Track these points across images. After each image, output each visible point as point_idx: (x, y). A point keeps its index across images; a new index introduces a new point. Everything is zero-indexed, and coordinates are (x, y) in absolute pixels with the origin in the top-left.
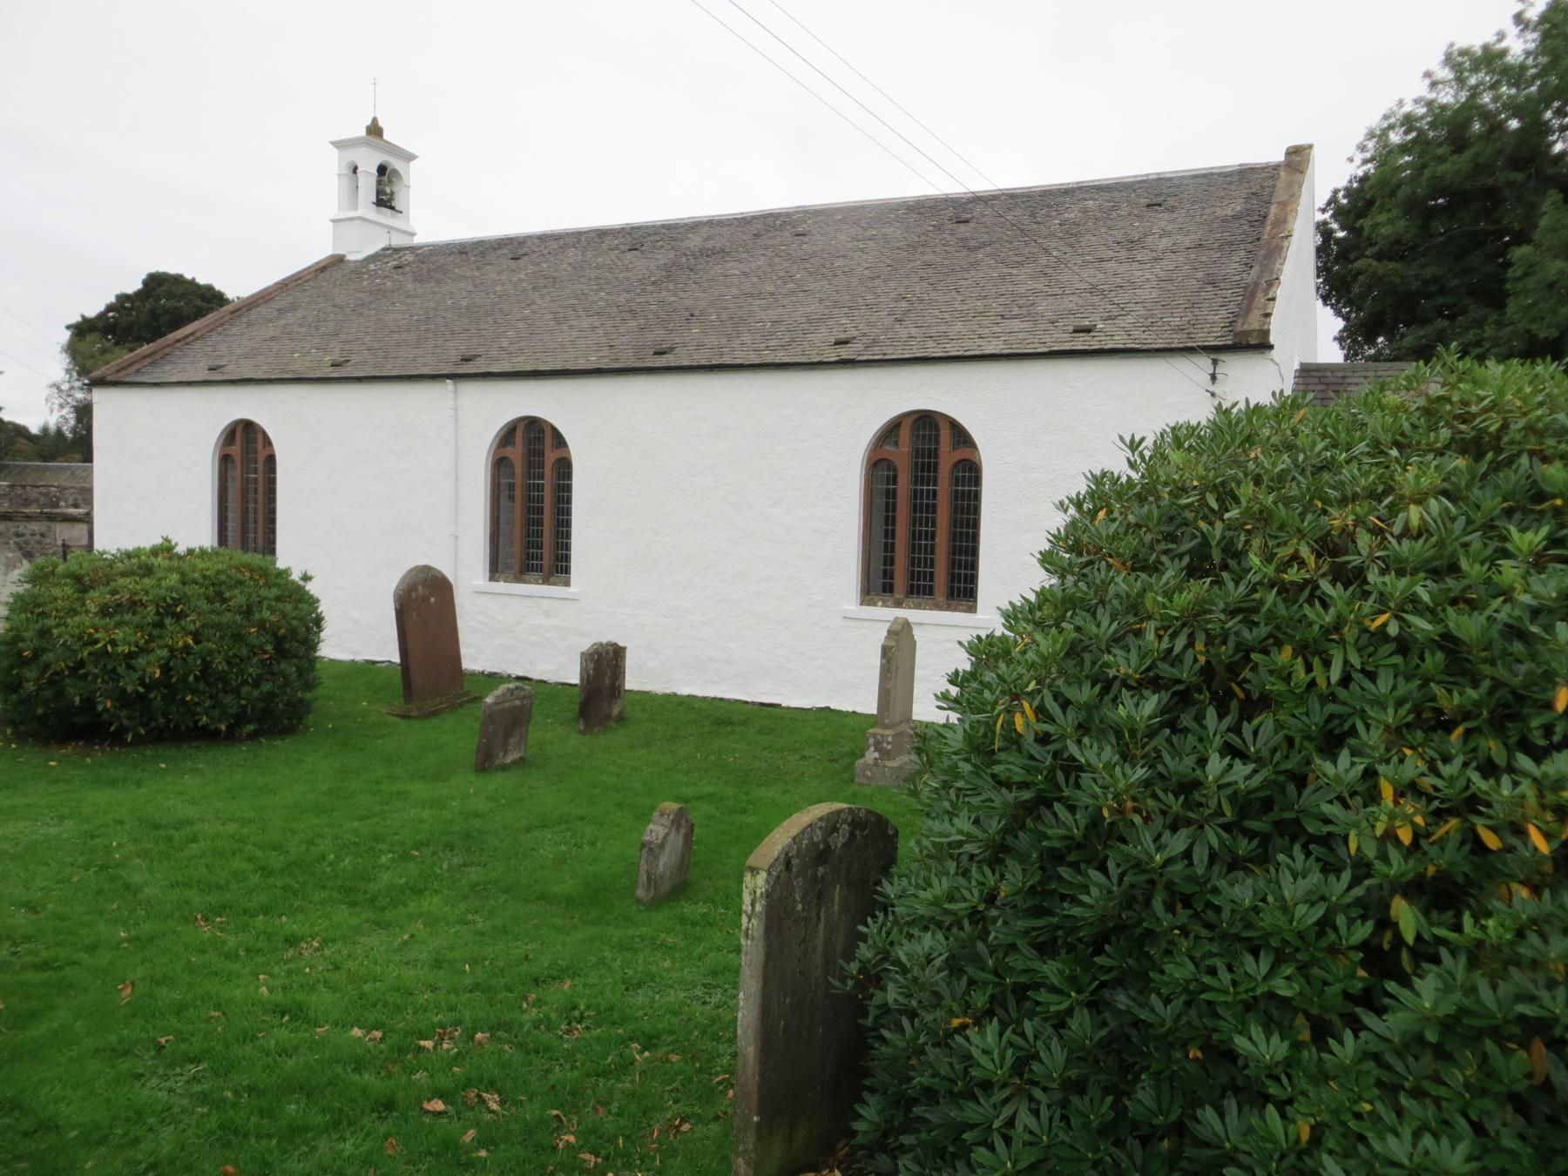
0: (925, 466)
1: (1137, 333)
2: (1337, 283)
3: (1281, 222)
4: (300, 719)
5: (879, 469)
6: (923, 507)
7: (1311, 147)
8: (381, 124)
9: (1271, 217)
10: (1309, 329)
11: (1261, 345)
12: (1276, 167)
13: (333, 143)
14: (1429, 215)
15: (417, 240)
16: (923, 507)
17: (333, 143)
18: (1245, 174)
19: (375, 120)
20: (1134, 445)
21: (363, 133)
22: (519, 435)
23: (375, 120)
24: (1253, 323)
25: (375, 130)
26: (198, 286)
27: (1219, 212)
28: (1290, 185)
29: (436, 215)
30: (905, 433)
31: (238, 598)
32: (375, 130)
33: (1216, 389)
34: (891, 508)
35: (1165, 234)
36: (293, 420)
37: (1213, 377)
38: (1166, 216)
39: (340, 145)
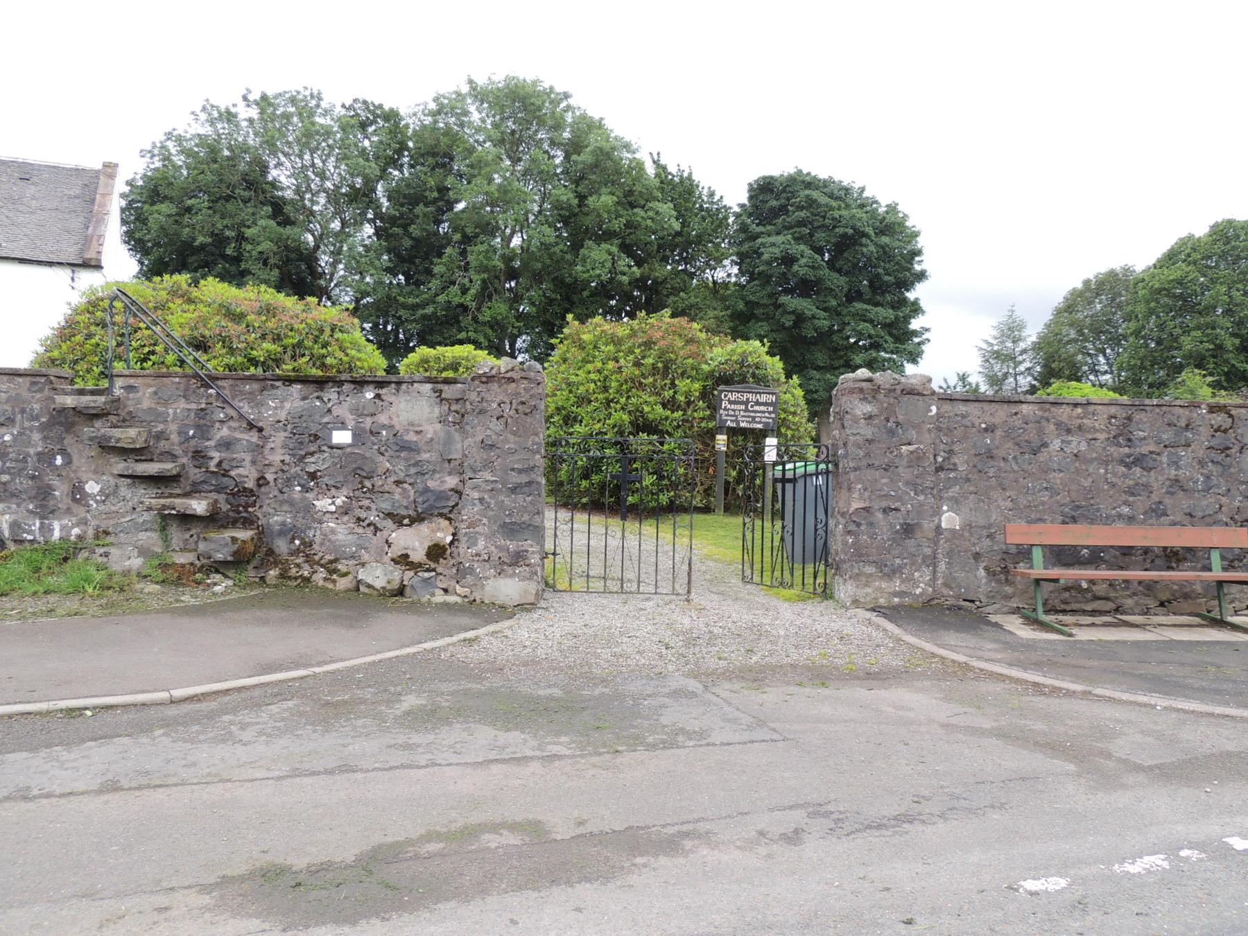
1: (27, 251)
2: (136, 242)
3: (103, 205)
4: (618, 172)
7: (116, 165)
9: (97, 201)
10: (120, 265)
11: (98, 267)
12: (98, 172)
14: (548, 95)
18: (78, 172)
20: (69, 304)
24: (90, 254)
26: (377, 914)
27: (66, 192)
28: (107, 185)
33: (74, 285)
35: (33, 198)
37: (73, 279)
38: (33, 187)
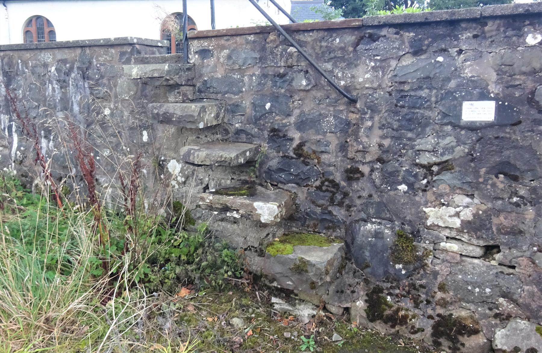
0: (40, 32)
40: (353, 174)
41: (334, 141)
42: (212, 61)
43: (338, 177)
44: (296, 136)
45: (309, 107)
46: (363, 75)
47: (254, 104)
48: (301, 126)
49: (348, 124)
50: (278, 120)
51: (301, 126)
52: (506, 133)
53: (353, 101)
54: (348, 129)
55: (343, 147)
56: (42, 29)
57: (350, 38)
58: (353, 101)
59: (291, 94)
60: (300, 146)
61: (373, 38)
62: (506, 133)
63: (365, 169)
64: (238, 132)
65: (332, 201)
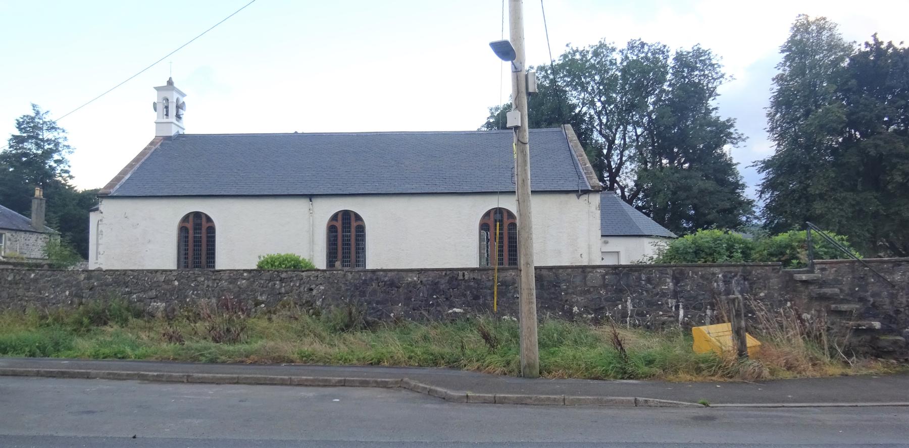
0: (197, 227)
5: (183, 229)
6: (197, 242)
8: (174, 80)
13: (155, 88)
15: (186, 132)
16: (346, 243)
17: (155, 88)
19: (170, 78)
21: (165, 84)
22: (492, 214)
23: (170, 78)
25: (170, 83)
29: (194, 124)
30: (191, 218)
31: (295, 325)
32: (170, 83)
34: (187, 242)
36: (370, 211)
39: (158, 89)
40: (897, 312)
41: (887, 301)
42: (827, 272)
43: (891, 313)
44: (872, 299)
45: (876, 289)
46: (898, 277)
47: (850, 289)
48: (873, 296)
49: (892, 294)
50: (862, 294)
51: (873, 296)
52: (718, 285)
53: (894, 286)
54: (893, 297)
55: (892, 303)
56: (201, 224)
57: (890, 265)
58: (894, 286)
59: (867, 284)
60: (874, 303)
61: (900, 265)
62: (718, 285)
63: (902, 310)
64: (842, 299)
65: (890, 322)
